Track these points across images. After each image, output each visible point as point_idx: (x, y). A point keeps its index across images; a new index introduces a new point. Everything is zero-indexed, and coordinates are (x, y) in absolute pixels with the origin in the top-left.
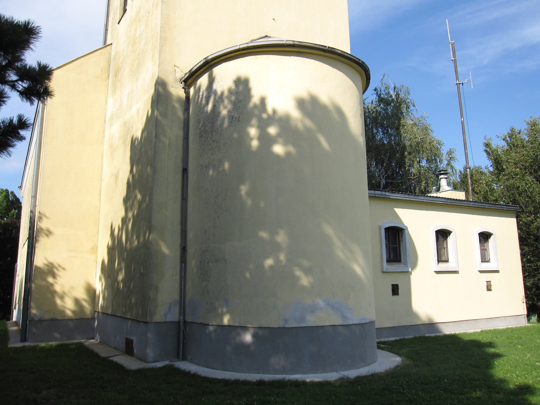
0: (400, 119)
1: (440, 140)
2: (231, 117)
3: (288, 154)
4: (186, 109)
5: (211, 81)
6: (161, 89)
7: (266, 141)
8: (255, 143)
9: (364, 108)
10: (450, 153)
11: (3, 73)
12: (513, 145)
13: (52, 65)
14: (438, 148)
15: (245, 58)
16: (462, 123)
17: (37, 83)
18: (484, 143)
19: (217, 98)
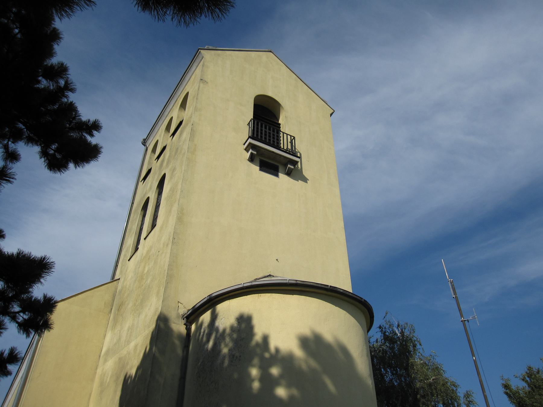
0: (408, 359)
1: (454, 381)
2: (232, 355)
3: (291, 398)
4: (186, 346)
5: (214, 317)
6: (162, 325)
7: (269, 383)
8: (256, 385)
9: (370, 347)
10: (467, 395)
11: (7, 304)
12: (535, 386)
13: (58, 298)
14: (453, 390)
15: (249, 296)
16: (475, 361)
17: (38, 317)
18: (503, 384)
19: (218, 336)
